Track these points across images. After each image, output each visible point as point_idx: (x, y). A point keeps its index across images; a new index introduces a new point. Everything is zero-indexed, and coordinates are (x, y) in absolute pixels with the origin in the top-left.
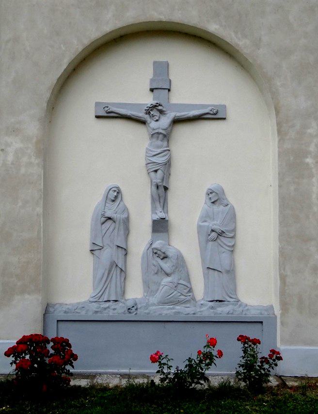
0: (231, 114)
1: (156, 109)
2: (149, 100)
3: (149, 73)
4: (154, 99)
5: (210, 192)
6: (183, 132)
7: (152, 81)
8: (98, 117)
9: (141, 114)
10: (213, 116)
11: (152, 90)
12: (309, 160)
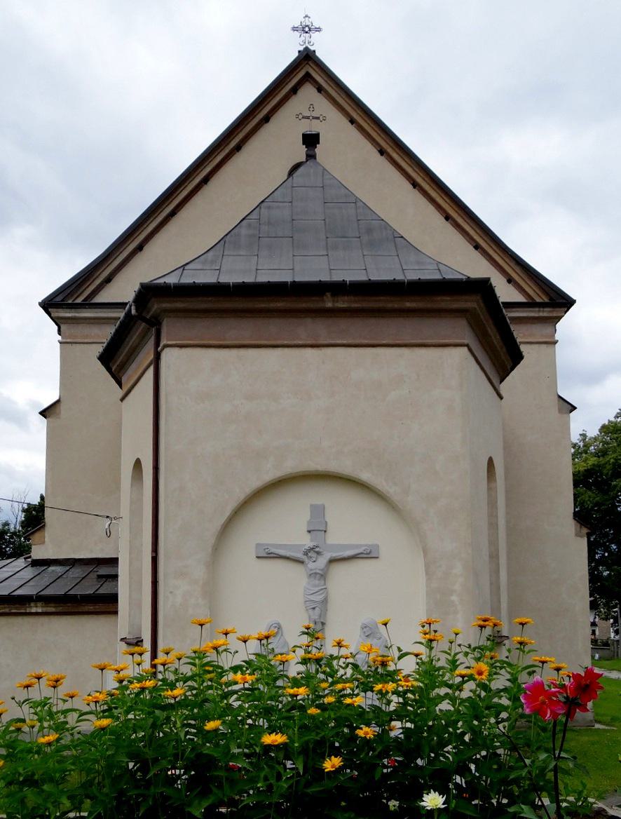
0: (383, 552)
1: (314, 551)
2: (307, 542)
3: (306, 516)
4: (312, 541)
5: (364, 627)
6: (339, 571)
7: (309, 523)
8: (258, 557)
9: (300, 555)
10: (368, 555)
11: (309, 532)
12: (454, 598)
